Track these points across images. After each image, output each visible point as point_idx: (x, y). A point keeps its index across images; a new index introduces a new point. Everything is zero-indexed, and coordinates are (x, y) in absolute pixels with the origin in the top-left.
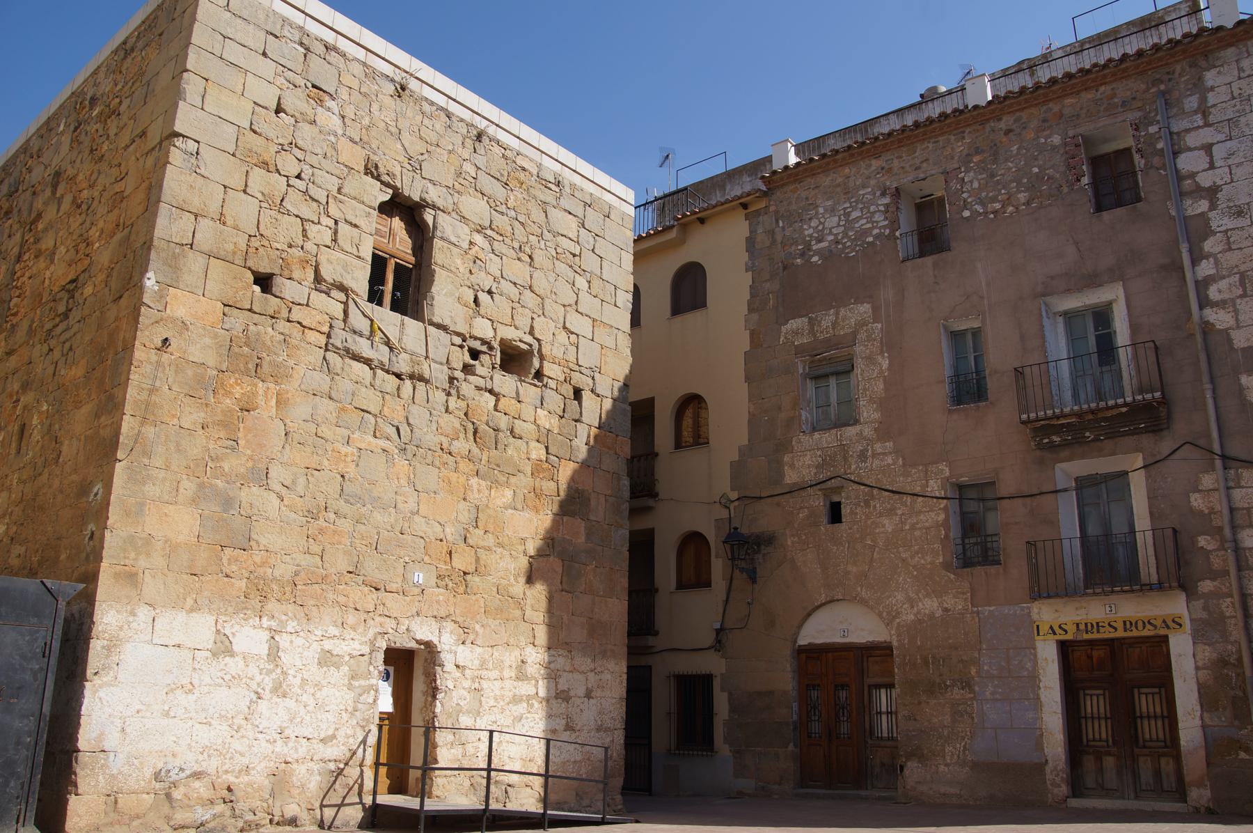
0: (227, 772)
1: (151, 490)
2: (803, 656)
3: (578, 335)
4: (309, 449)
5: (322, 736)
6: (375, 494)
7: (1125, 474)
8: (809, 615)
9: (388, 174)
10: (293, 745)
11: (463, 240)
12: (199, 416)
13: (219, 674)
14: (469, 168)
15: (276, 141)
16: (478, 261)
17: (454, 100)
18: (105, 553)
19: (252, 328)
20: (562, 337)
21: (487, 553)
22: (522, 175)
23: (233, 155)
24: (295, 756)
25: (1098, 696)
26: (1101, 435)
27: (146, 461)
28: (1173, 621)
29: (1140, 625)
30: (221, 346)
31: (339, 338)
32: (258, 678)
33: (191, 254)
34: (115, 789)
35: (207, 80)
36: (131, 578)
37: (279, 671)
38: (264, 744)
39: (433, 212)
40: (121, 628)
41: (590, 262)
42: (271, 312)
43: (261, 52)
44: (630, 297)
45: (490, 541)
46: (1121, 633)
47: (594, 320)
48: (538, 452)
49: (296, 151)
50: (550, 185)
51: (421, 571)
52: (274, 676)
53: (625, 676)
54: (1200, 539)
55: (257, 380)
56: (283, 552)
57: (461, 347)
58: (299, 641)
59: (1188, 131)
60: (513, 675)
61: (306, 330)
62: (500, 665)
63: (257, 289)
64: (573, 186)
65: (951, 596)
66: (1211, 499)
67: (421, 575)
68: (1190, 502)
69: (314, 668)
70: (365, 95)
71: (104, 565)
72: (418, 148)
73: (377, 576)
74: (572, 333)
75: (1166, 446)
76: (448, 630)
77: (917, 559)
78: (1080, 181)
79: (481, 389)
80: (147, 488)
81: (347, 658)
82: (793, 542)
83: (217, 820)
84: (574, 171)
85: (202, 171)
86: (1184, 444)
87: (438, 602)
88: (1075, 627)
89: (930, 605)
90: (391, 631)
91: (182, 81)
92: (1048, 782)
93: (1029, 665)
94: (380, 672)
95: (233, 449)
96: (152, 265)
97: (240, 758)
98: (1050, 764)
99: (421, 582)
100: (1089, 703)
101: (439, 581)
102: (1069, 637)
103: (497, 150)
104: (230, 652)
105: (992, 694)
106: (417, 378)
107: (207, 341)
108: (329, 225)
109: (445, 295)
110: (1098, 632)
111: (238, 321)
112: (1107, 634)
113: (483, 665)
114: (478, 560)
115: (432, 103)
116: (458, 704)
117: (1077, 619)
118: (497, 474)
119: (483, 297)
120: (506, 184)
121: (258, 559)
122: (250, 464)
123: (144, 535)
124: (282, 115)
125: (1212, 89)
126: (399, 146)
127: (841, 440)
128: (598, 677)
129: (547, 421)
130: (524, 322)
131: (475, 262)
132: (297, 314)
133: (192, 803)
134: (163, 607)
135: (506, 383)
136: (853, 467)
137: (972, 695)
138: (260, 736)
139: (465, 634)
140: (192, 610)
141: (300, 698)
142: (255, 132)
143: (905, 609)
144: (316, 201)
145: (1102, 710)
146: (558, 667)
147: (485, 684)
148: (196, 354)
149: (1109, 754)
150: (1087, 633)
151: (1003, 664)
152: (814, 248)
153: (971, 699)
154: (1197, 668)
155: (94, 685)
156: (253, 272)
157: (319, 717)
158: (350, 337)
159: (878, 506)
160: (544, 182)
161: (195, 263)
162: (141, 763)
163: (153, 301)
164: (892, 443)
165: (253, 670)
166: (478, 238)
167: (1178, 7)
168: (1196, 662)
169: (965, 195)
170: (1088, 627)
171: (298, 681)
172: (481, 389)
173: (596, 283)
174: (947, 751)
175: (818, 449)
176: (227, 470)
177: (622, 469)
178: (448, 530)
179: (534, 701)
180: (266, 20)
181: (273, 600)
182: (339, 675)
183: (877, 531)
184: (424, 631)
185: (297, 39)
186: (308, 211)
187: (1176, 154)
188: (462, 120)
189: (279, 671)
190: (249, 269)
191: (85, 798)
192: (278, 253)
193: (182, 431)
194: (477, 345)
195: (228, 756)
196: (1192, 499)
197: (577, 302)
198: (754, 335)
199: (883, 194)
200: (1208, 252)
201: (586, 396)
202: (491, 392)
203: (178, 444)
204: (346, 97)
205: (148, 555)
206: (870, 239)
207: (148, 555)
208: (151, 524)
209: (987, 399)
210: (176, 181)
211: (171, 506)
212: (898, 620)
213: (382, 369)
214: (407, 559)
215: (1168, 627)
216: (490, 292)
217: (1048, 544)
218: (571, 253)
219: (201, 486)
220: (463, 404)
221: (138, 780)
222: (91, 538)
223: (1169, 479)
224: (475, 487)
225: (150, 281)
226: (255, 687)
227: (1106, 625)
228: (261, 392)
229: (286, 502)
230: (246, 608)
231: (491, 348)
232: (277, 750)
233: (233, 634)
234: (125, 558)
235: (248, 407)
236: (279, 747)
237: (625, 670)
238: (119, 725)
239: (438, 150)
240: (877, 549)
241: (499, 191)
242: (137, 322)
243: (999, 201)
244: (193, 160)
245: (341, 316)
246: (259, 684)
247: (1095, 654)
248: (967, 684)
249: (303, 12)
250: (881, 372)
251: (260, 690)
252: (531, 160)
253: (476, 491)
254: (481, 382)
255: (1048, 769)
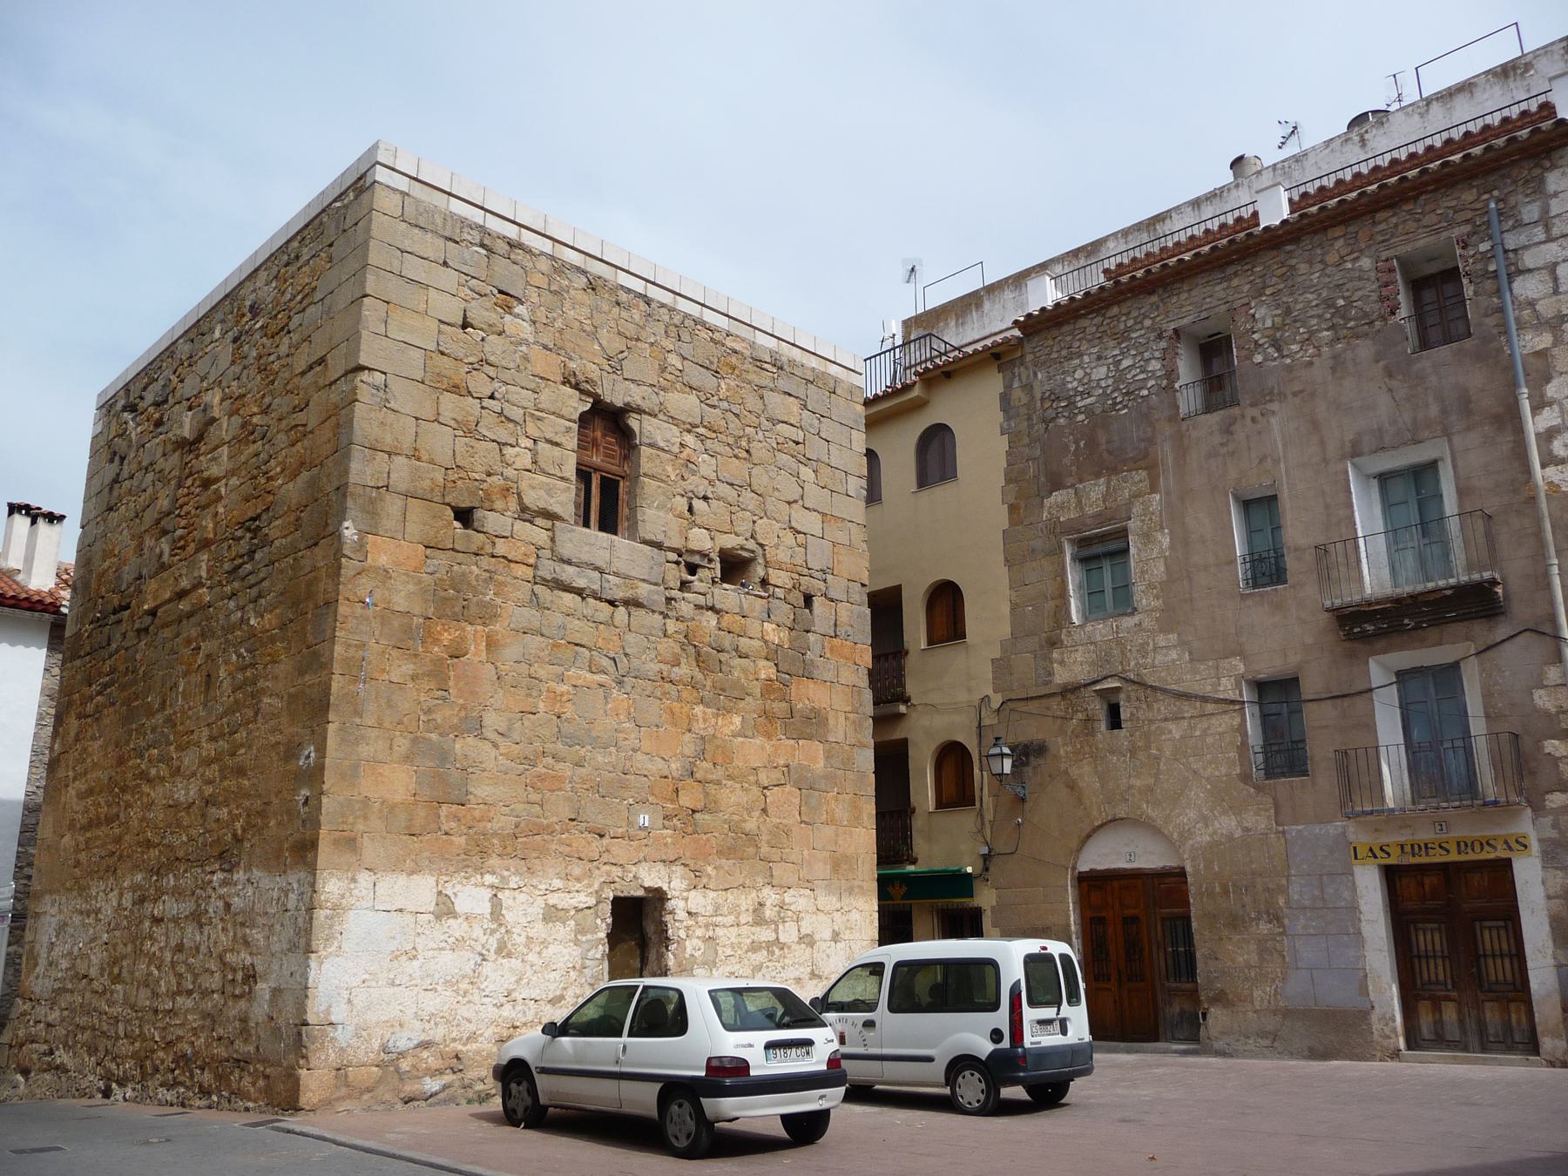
0: (454, 1040)
1: (365, 750)
2: (1085, 885)
3: (805, 534)
4: (523, 692)
5: (550, 997)
6: (594, 734)
7: (1455, 666)
8: (1089, 836)
9: (587, 382)
10: (520, 1008)
11: (673, 444)
12: (409, 668)
13: (442, 937)
14: (674, 360)
15: (466, 361)
16: (690, 465)
17: (653, 283)
18: (323, 818)
19: (456, 568)
20: (789, 538)
21: (716, 787)
22: (734, 360)
23: (423, 383)
24: (523, 1020)
25: (1432, 930)
26: (1425, 622)
27: (358, 720)
28: (1517, 842)
29: (1477, 845)
30: (425, 591)
31: (548, 569)
32: (483, 939)
33: (388, 497)
34: (345, 1062)
35: (388, 303)
36: (350, 843)
37: (503, 930)
38: (491, 1008)
39: (638, 417)
40: (343, 896)
41: (815, 449)
42: (474, 548)
43: (441, 262)
44: (864, 483)
45: (719, 773)
46: (1454, 857)
47: (824, 515)
48: (766, 670)
49: (487, 368)
50: (766, 366)
51: (646, 813)
52: (498, 935)
53: (876, 915)
54: (1546, 743)
55: (464, 624)
56: (501, 804)
57: (677, 563)
58: (522, 897)
59: (1525, 247)
60: (750, 919)
61: (512, 565)
62: (735, 910)
63: (457, 524)
64: (792, 362)
65: (1252, 813)
66: (1559, 696)
67: (647, 817)
68: (1533, 700)
69: (539, 926)
70: (555, 293)
71: (323, 832)
72: (617, 345)
73: (600, 821)
74: (799, 533)
75: (1502, 631)
76: (678, 874)
77: (1209, 770)
78: (1394, 314)
79: (702, 607)
80: (360, 749)
81: (573, 912)
82: (1067, 752)
83: (447, 1091)
84: (793, 345)
85: (392, 405)
86: (1525, 630)
87: (666, 844)
88: (1399, 849)
89: (1227, 824)
90: (617, 879)
91: (363, 308)
92: (1375, 1033)
93: (1346, 894)
94: (608, 925)
95: (445, 699)
96: (351, 513)
97: (468, 1025)
98: (1377, 1010)
99: (646, 825)
100: (1421, 938)
101: (666, 822)
102: (1392, 861)
103: (704, 334)
104: (451, 913)
105: (1305, 927)
106: (633, 603)
107: (411, 587)
108: (528, 446)
109: (657, 507)
110: (1427, 854)
111: (440, 561)
112: (1438, 857)
113: (717, 911)
114: (707, 794)
115: (629, 291)
116: (692, 955)
117: (1402, 839)
118: (726, 697)
119: (698, 504)
120: (717, 372)
121: (477, 814)
122: (463, 714)
123: (361, 798)
124: (469, 330)
125: (1556, 194)
126: (597, 347)
127: (1117, 632)
128: (845, 918)
129: (774, 634)
130: (744, 527)
131: (687, 466)
132: (501, 548)
133: (420, 1074)
134: (384, 871)
135: (728, 595)
136: (1132, 663)
137: (1281, 930)
138: (486, 1000)
139: (697, 880)
140: (413, 873)
141: (526, 958)
142: (442, 353)
143: (1199, 829)
144: (512, 421)
145: (1438, 947)
146: (800, 908)
147: (720, 932)
148: (400, 603)
149: (1448, 999)
150: (1414, 856)
151: (1316, 893)
152: (1079, 405)
153: (1281, 934)
154: (1549, 897)
155: (320, 957)
156: (453, 508)
157: (546, 976)
158: (559, 567)
159: (1162, 708)
160: (758, 364)
161: (393, 505)
162: (369, 1035)
163: (352, 552)
164: (1176, 635)
165: (477, 932)
166: (690, 439)
167: (1549, 49)
168: (1546, 890)
169: (1256, 336)
170: (1415, 848)
171: (522, 939)
172: (702, 607)
173: (824, 470)
174: (1255, 996)
175: (1091, 643)
176: (439, 721)
177: (864, 682)
178: (673, 766)
179: (775, 948)
180: (444, 224)
181: (494, 855)
182: (563, 931)
183: (1163, 737)
184: (652, 877)
185: (478, 241)
186: (503, 434)
187: (1511, 278)
188: (663, 306)
189: (503, 930)
190: (448, 504)
191: (317, 1073)
192: (477, 483)
193: (393, 685)
194: (696, 559)
195: (455, 1023)
196: (1536, 696)
197: (802, 496)
198: (1013, 509)
199: (1160, 337)
200: (1552, 397)
201: (817, 602)
202: (712, 609)
203: (389, 701)
204: (535, 299)
205: (366, 818)
206: (1145, 392)
207: (366, 818)
208: (367, 786)
209: (1285, 582)
210: (366, 420)
211: (386, 766)
212: (1191, 842)
213: (596, 598)
214: (631, 801)
215: (1510, 848)
216: (705, 498)
217: (1361, 752)
218: (794, 442)
219: (415, 741)
220: (682, 626)
221: (367, 1053)
222: (306, 802)
223: (1507, 673)
224: (700, 715)
225: (349, 531)
226: (479, 949)
227: (1437, 847)
228: (470, 637)
229: (502, 750)
230: (468, 866)
231: (710, 561)
232: (505, 1014)
233: (455, 894)
234: (343, 822)
235: (456, 653)
236: (507, 1011)
237: (876, 908)
238: (346, 996)
239: (639, 344)
240: (1163, 759)
241: (709, 381)
242: (338, 575)
243: (1297, 343)
244: (381, 394)
245: (548, 544)
246: (483, 946)
247: (1427, 881)
248: (1276, 918)
249: (482, 208)
250: (1162, 551)
251: (484, 952)
252: (743, 340)
253: (701, 721)
254: (701, 600)
255: (1374, 1017)
